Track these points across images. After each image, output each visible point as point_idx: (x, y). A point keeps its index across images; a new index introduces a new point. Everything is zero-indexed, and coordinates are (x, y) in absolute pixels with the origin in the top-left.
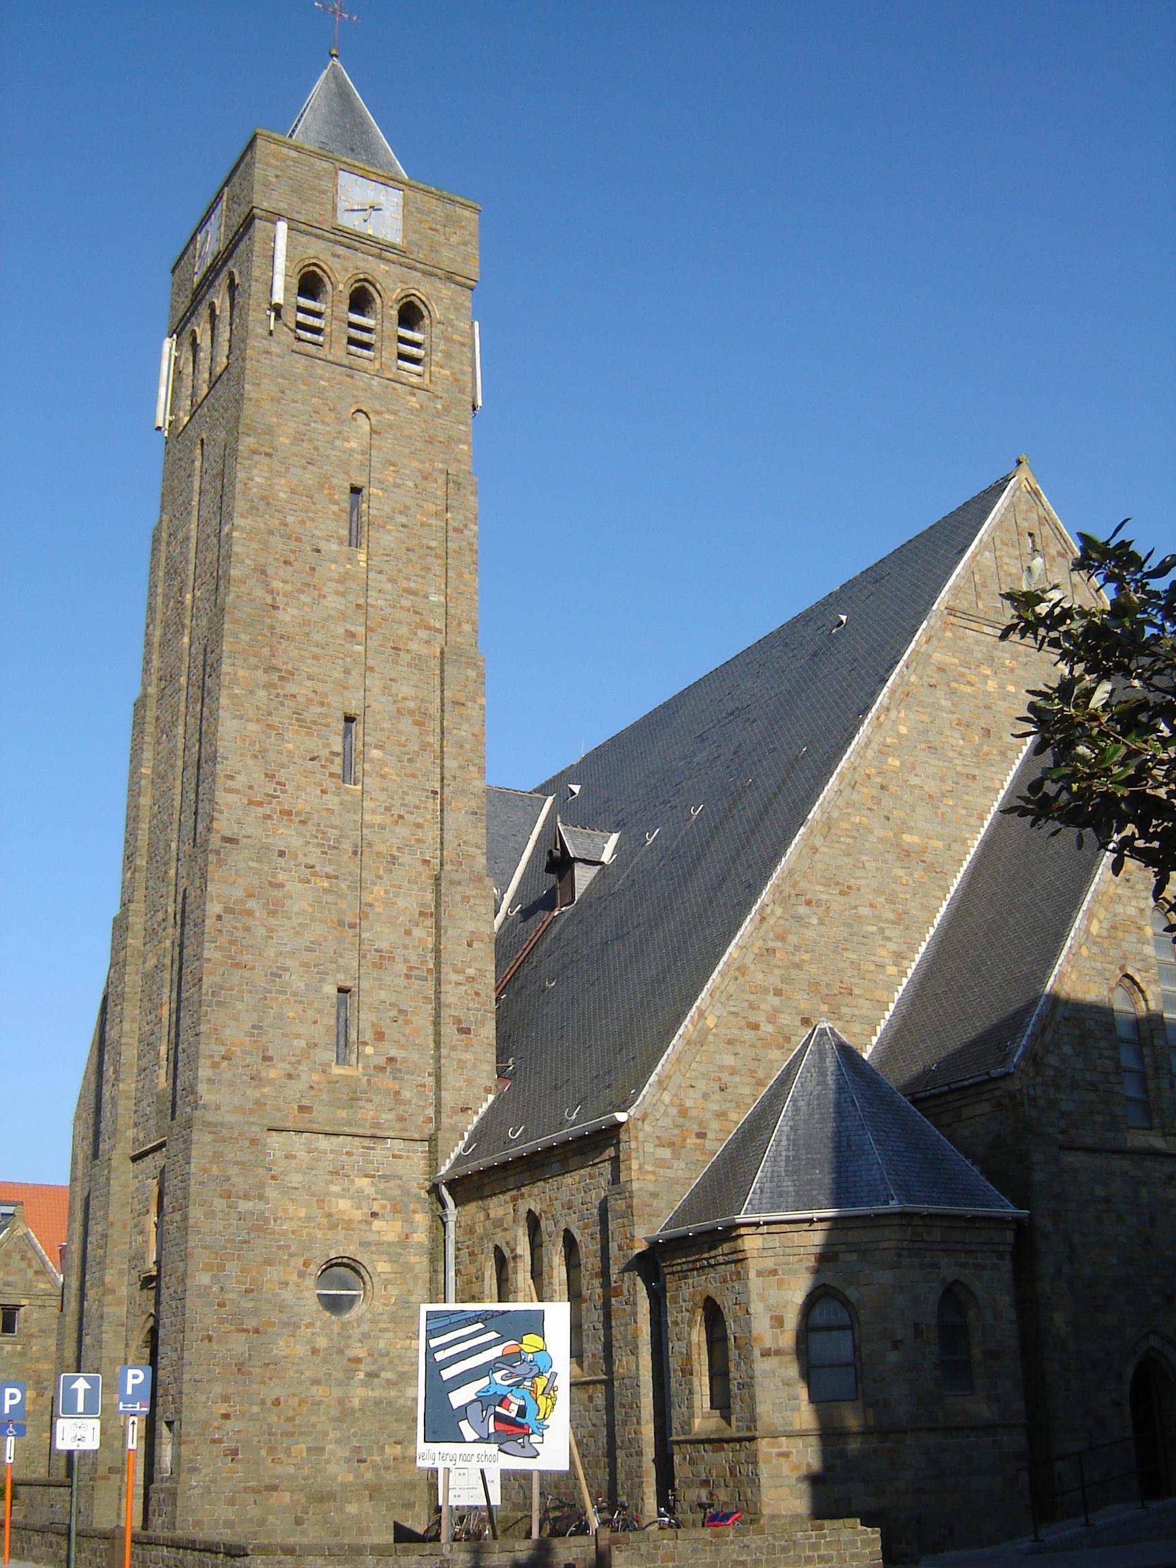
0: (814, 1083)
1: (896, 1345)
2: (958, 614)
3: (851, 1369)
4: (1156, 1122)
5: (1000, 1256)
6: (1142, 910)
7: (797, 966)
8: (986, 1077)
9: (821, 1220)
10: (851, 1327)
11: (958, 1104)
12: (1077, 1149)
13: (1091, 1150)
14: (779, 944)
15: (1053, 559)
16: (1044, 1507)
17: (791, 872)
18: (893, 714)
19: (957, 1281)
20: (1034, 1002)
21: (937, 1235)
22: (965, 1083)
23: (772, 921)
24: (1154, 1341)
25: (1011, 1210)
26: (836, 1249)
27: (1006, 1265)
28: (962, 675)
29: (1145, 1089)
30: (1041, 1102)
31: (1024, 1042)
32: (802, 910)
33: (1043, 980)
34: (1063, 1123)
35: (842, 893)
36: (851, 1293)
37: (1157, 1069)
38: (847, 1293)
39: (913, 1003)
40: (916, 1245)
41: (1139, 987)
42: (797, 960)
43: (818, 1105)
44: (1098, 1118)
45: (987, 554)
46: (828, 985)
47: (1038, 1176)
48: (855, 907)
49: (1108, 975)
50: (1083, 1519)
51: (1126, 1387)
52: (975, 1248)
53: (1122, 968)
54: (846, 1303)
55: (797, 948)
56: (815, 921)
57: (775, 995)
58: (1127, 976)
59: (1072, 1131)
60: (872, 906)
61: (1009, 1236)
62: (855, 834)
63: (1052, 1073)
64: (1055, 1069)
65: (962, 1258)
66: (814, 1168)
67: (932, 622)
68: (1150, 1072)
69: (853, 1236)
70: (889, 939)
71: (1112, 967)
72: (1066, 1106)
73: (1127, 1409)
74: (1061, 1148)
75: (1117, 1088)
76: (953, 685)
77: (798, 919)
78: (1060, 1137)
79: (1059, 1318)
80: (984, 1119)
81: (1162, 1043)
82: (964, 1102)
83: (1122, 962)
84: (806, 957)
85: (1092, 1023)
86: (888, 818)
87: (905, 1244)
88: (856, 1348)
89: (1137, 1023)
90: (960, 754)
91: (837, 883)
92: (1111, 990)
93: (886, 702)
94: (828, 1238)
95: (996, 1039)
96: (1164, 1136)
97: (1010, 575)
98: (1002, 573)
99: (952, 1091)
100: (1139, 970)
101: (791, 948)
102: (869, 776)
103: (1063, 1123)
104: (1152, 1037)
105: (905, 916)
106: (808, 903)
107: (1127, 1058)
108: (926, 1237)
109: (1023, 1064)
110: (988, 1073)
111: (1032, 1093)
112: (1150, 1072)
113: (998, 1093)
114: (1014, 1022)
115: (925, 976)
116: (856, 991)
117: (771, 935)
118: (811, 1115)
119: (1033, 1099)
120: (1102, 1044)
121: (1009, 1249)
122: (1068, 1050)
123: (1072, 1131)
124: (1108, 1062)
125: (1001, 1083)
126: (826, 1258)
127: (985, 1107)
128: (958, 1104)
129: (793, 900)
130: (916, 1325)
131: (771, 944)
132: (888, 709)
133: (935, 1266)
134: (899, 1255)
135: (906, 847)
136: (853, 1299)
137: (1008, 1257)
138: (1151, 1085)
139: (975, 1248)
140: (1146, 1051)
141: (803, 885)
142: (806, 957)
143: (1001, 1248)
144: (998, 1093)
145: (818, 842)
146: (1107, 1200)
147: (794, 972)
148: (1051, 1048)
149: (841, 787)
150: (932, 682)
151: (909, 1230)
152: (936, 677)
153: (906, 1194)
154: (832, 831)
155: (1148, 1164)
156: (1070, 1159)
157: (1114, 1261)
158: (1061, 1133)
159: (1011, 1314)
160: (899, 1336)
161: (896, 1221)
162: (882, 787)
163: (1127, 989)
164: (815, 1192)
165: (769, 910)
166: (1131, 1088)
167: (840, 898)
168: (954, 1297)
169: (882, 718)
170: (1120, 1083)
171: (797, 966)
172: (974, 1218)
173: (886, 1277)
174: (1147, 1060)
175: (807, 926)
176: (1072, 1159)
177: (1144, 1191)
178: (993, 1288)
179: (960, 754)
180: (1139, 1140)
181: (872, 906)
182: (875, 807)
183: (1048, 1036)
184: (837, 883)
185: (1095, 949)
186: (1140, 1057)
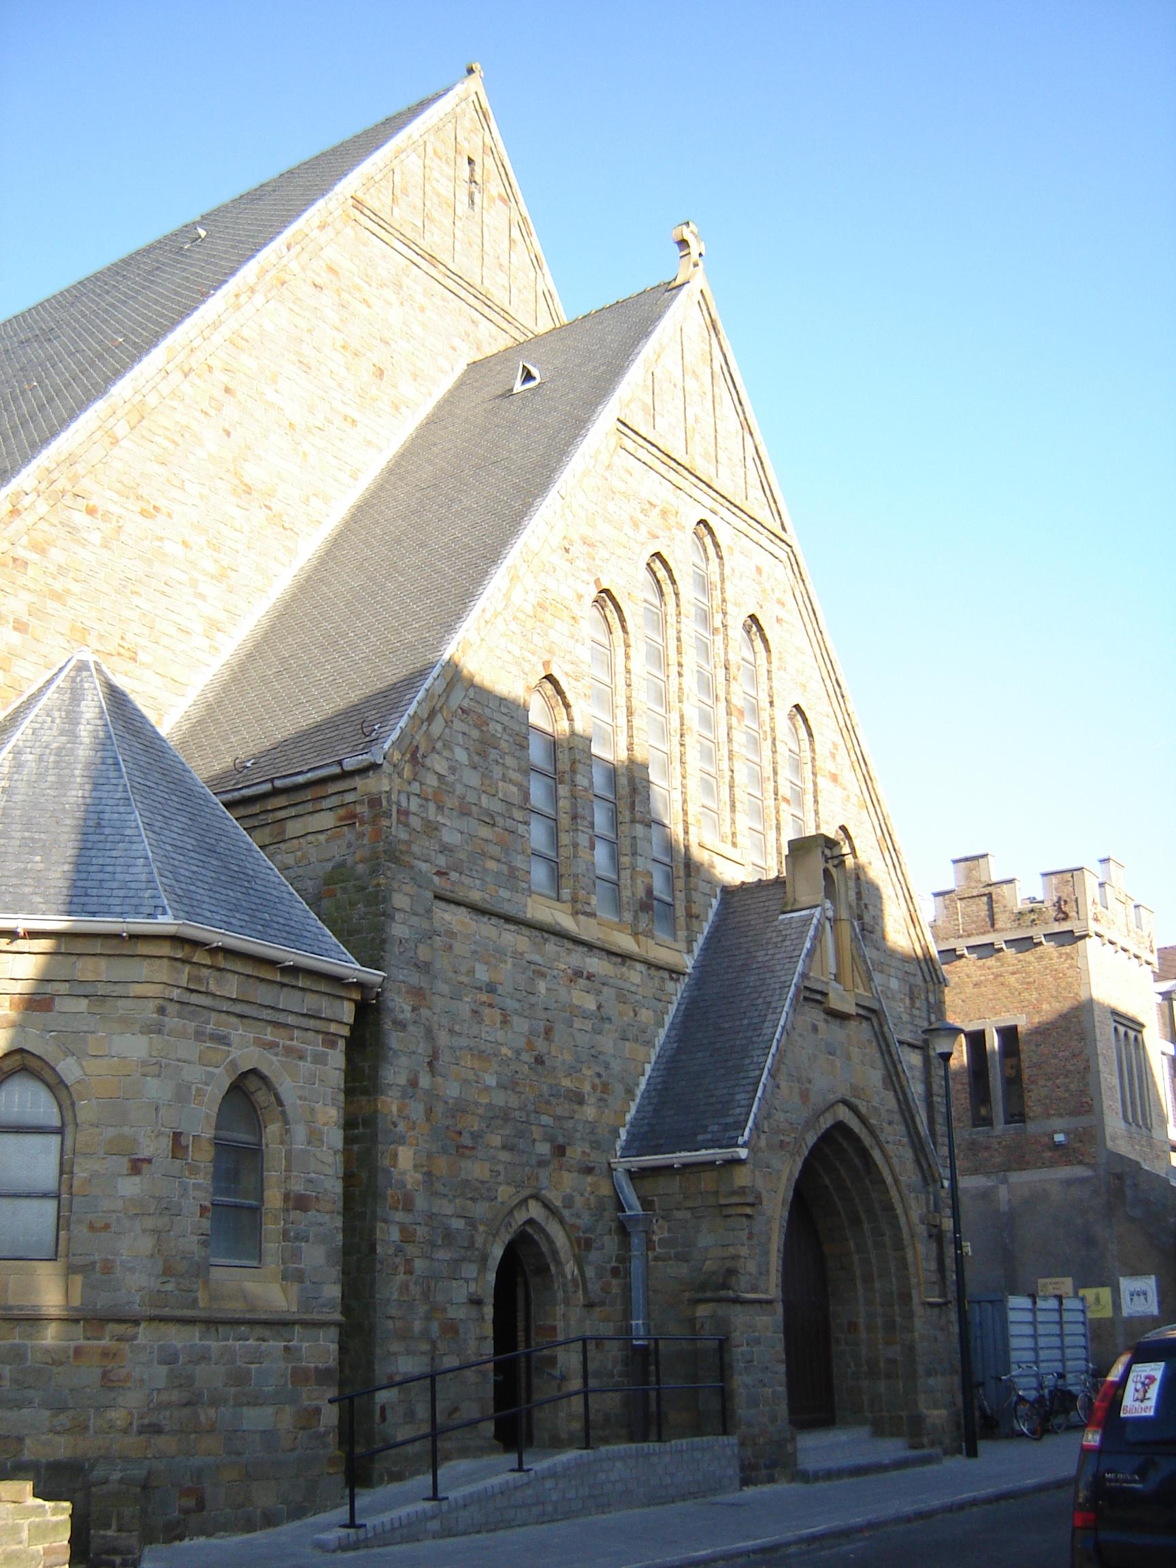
0: (55, 732)
1: (136, 1166)
2: (366, 211)
3: (50, 1206)
4: (566, 893)
5: (330, 1040)
6: (580, 597)
7: (56, 596)
8: (336, 770)
9: (33, 935)
10: (60, 1131)
11: (281, 814)
12: (458, 904)
13: (477, 910)
14: (33, 556)
15: (492, 200)
16: (360, 1460)
17: (71, 460)
18: (259, 299)
19: (254, 1072)
20: (422, 673)
21: (231, 987)
22: (300, 779)
23: (29, 518)
24: (535, 1210)
25: (351, 968)
26: (50, 988)
27: (337, 1057)
28: (359, 289)
29: (555, 842)
30: (415, 822)
31: (402, 724)
32: (80, 518)
33: (441, 641)
34: (442, 861)
35: (143, 513)
36: (69, 1069)
37: (574, 817)
38: (61, 1067)
39: (225, 688)
40: (194, 999)
41: (564, 698)
42: (58, 586)
43: (56, 762)
44: (492, 865)
45: (413, 157)
46: (101, 637)
47: (398, 930)
48: (161, 539)
49: (527, 667)
50: (426, 1479)
51: (491, 1277)
52: (290, 1020)
53: (546, 664)
54: (56, 1086)
55: (62, 570)
56: (96, 538)
57: (15, 629)
58: (549, 678)
59: (454, 875)
60: (185, 544)
61: (347, 1012)
62: (178, 439)
63: (435, 783)
64: (441, 777)
65: (269, 1035)
66: (33, 852)
67: (332, 205)
68: (565, 820)
69: (87, 969)
70: (202, 597)
71: (534, 659)
72: (450, 837)
73: (489, 1311)
74: (437, 897)
75: (521, 829)
76: (345, 295)
77: (72, 530)
78: (436, 879)
79: (406, 1158)
80: (322, 837)
81: (585, 783)
82: (293, 812)
83: (547, 657)
84: (75, 588)
85: (499, 728)
86: (228, 434)
87: (175, 993)
88: (65, 1168)
89: (554, 745)
90: (340, 385)
91: (139, 498)
92: (529, 689)
93: (252, 280)
94: (48, 968)
95: (362, 720)
96: (575, 913)
97: (438, 195)
98: (428, 188)
99: (276, 792)
100: (567, 675)
101: (53, 569)
102: (210, 368)
103: (442, 861)
104: (573, 771)
105: (232, 574)
106: (91, 511)
107: (538, 792)
108: (213, 987)
109: (397, 756)
110: (340, 763)
111: (404, 804)
112: (565, 820)
113: (350, 797)
114: (390, 699)
115: (250, 656)
116: (142, 656)
117: (25, 540)
118: (41, 776)
119: (404, 813)
120: (509, 761)
121: (346, 1031)
122: (461, 756)
123: (454, 875)
124: (515, 789)
125: (358, 782)
126: (37, 1002)
127: (327, 820)
128: (281, 814)
129: (68, 500)
130: (177, 1136)
131: (21, 553)
132: (253, 291)
133: (223, 1040)
134: (161, 1011)
135: (249, 482)
136: (69, 1079)
137: (341, 1044)
138: (565, 839)
139: (290, 1020)
140: (563, 790)
141: (86, 484)
142: (75, 588)
143: (333, 1028)
144: (350, 797)
145: (121, 430)
146: (491, 988)
147: (51, 605)
148: (439, 745)
149: (169, 368)
150: (319, 281)
151: (187, 968)
152: (324, 278)
153: (187, 905)
154: (145, 423)
155: (551, 947)
156: (447, 917)
157: (491, 1081)
158: (439, 873)
159: (336, 1137)
160: (145, 1153)
161: (165, 949)
162: (227, 390)
163: (546, 699)
164: (27, 890)
165: (26, 501)
166: (537, 835)
167: (140, 519)
168: (246, 1094)
169: (243, 299)
170: (527, 823)
171: (56, 596)
172: (295, 970)
173: (136, 1046)
174: (561, 803)
175: (84, 543)
176: (449, 916)
177: (542, 986)
178: (311, 1089)
179: (340, 385)
180: (542, 910)
181: (185, 544)
182: (212, 412)
183: (437, 727)
184: (139, 498)
185: (514, 626)
186: (554, 798)
